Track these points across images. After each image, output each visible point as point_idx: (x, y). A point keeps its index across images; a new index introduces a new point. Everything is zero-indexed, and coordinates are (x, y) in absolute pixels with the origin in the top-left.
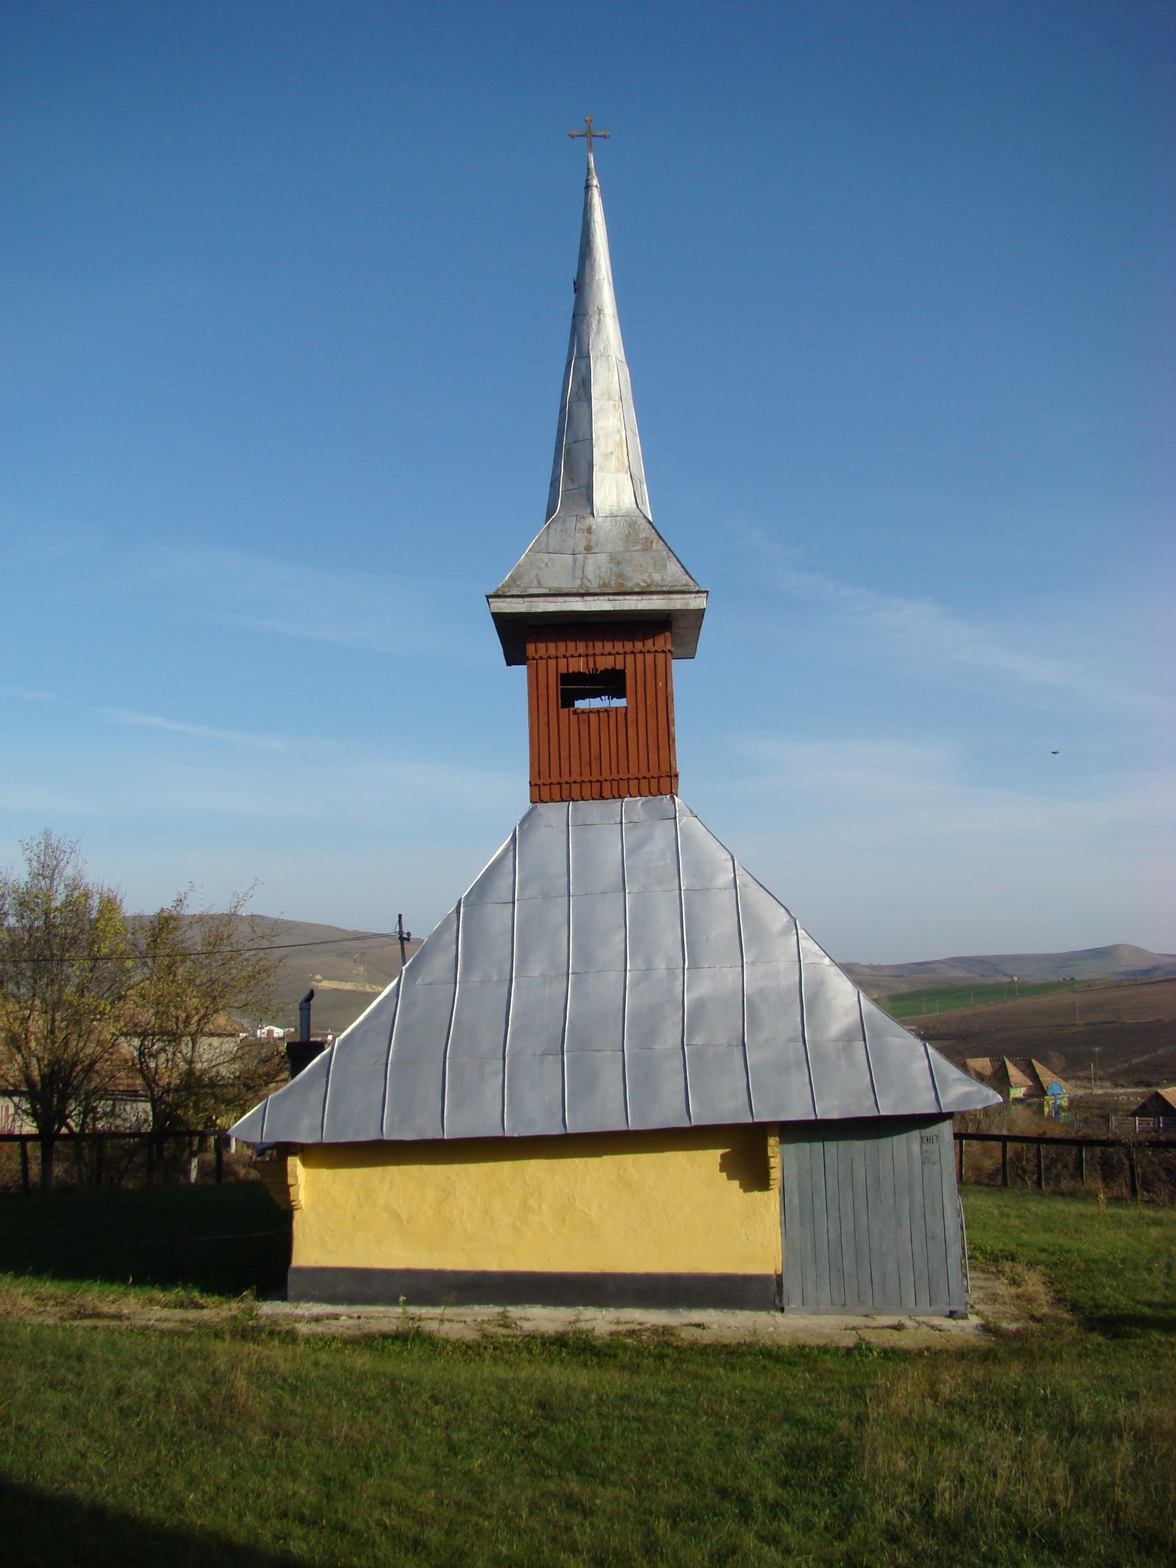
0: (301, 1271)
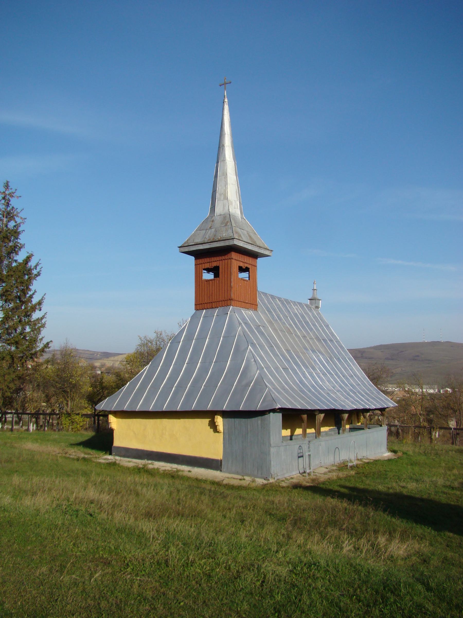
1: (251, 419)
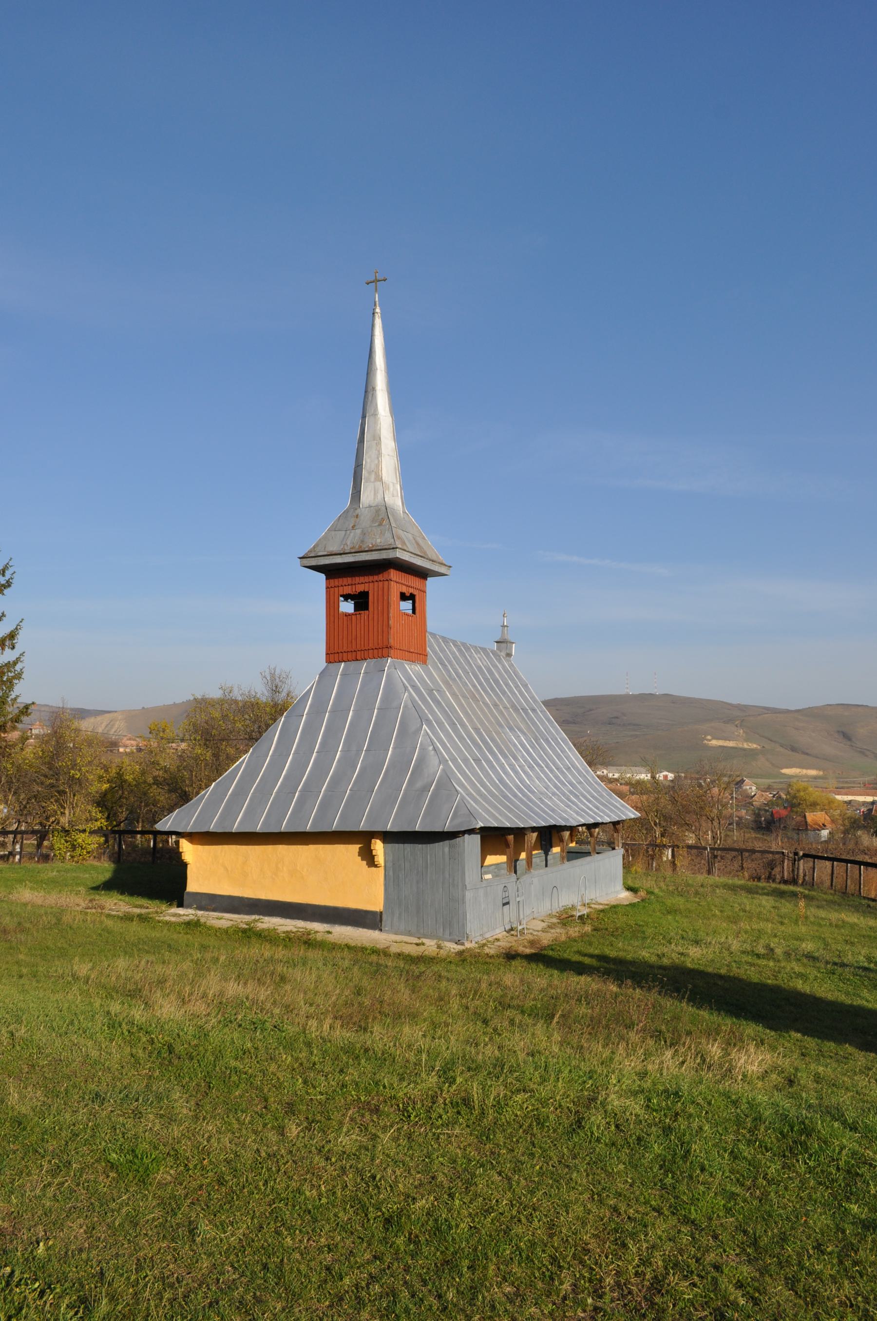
0: (189, 893)
1: (431, 845)
